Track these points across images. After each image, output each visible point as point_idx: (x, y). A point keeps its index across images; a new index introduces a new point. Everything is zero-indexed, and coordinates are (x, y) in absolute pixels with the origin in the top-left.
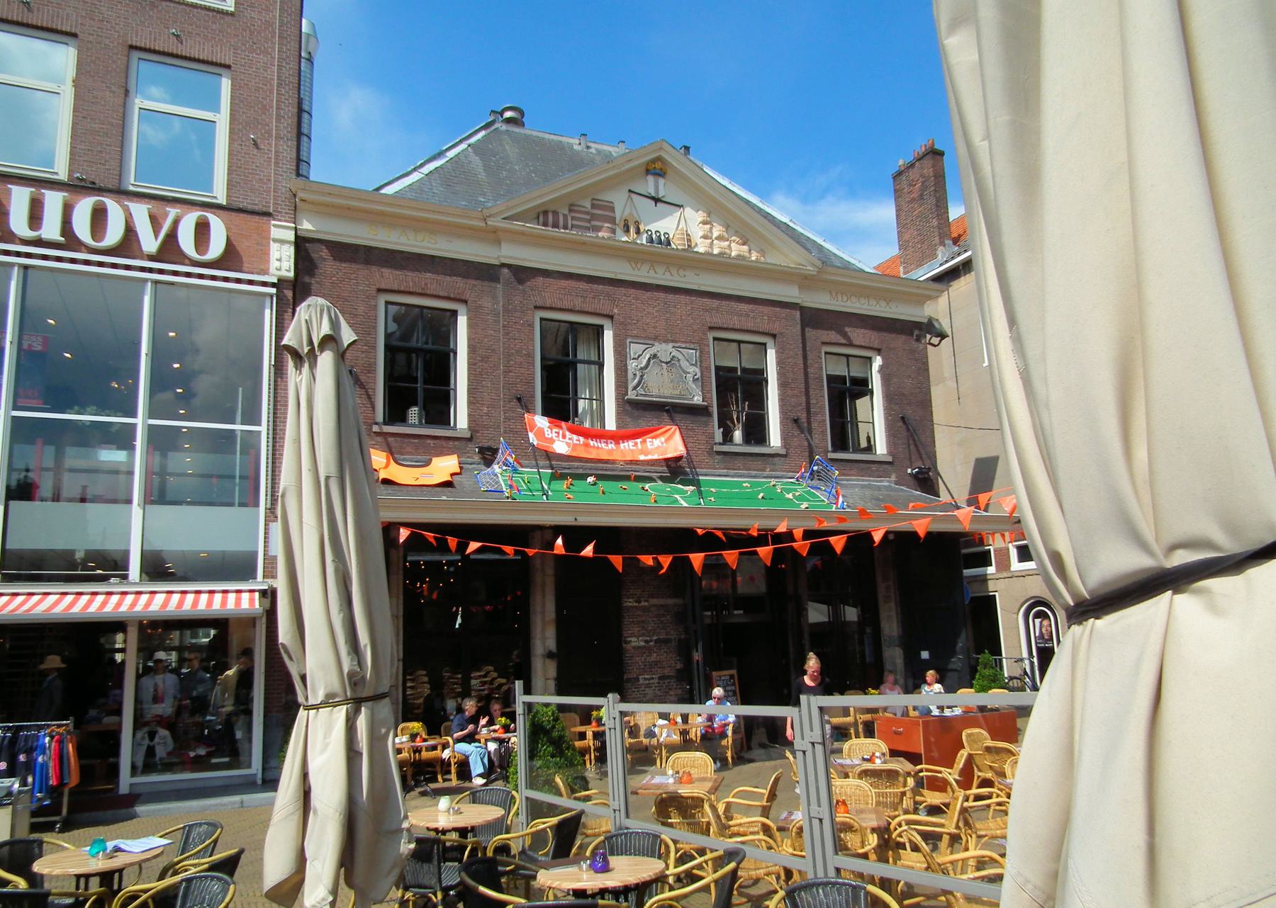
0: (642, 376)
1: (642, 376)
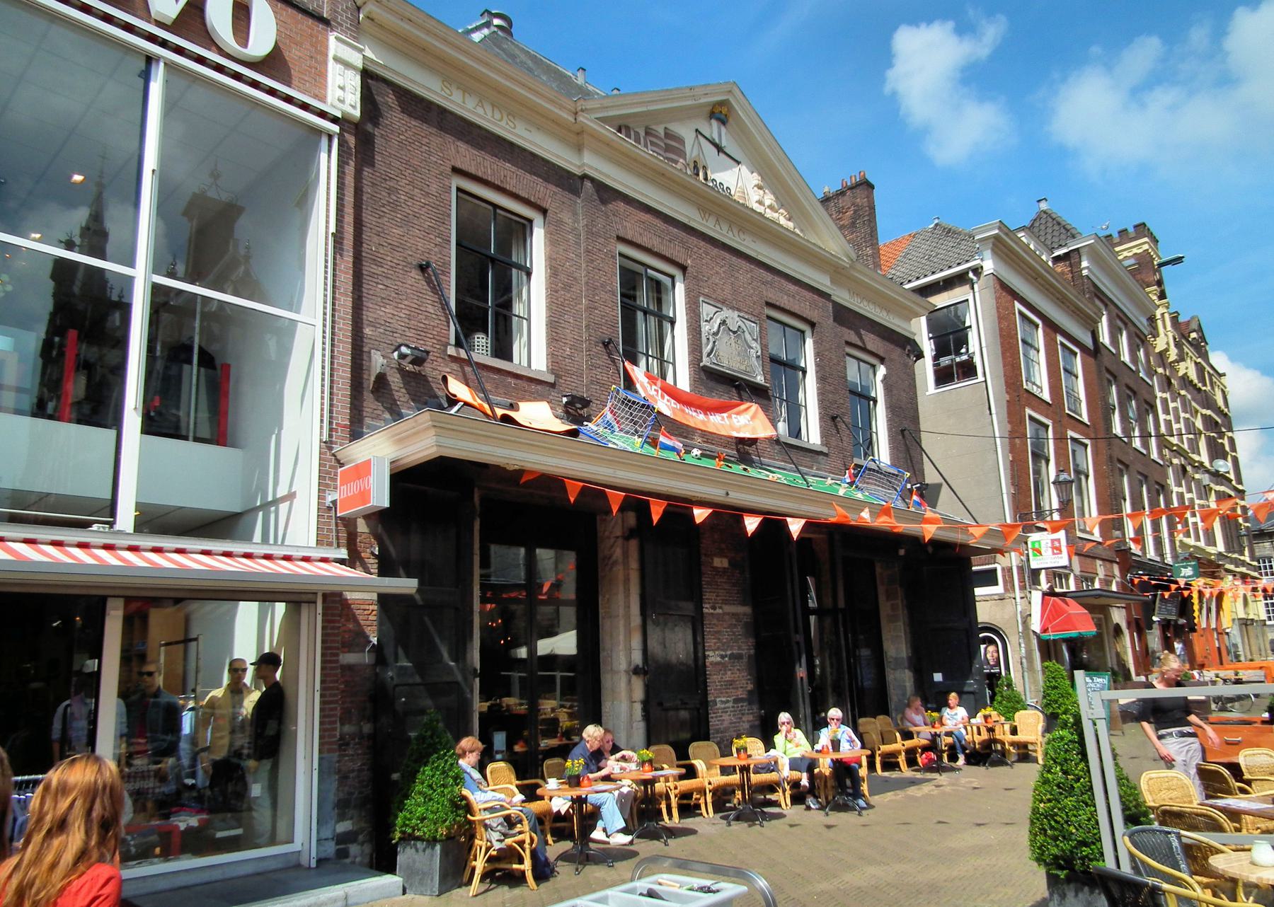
0: (714, 342)
1: (714, 342)
